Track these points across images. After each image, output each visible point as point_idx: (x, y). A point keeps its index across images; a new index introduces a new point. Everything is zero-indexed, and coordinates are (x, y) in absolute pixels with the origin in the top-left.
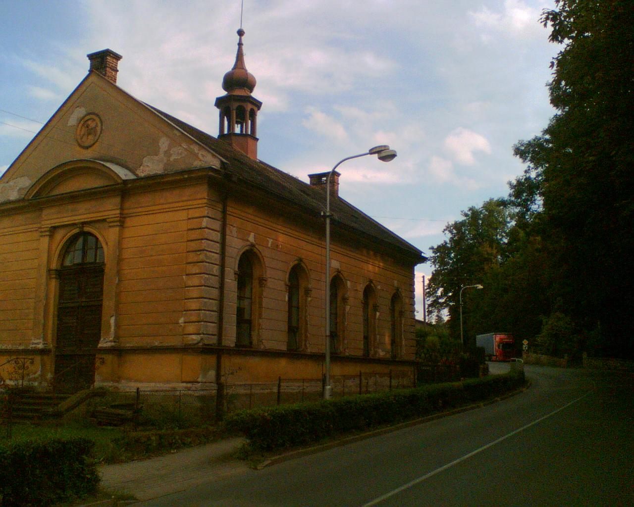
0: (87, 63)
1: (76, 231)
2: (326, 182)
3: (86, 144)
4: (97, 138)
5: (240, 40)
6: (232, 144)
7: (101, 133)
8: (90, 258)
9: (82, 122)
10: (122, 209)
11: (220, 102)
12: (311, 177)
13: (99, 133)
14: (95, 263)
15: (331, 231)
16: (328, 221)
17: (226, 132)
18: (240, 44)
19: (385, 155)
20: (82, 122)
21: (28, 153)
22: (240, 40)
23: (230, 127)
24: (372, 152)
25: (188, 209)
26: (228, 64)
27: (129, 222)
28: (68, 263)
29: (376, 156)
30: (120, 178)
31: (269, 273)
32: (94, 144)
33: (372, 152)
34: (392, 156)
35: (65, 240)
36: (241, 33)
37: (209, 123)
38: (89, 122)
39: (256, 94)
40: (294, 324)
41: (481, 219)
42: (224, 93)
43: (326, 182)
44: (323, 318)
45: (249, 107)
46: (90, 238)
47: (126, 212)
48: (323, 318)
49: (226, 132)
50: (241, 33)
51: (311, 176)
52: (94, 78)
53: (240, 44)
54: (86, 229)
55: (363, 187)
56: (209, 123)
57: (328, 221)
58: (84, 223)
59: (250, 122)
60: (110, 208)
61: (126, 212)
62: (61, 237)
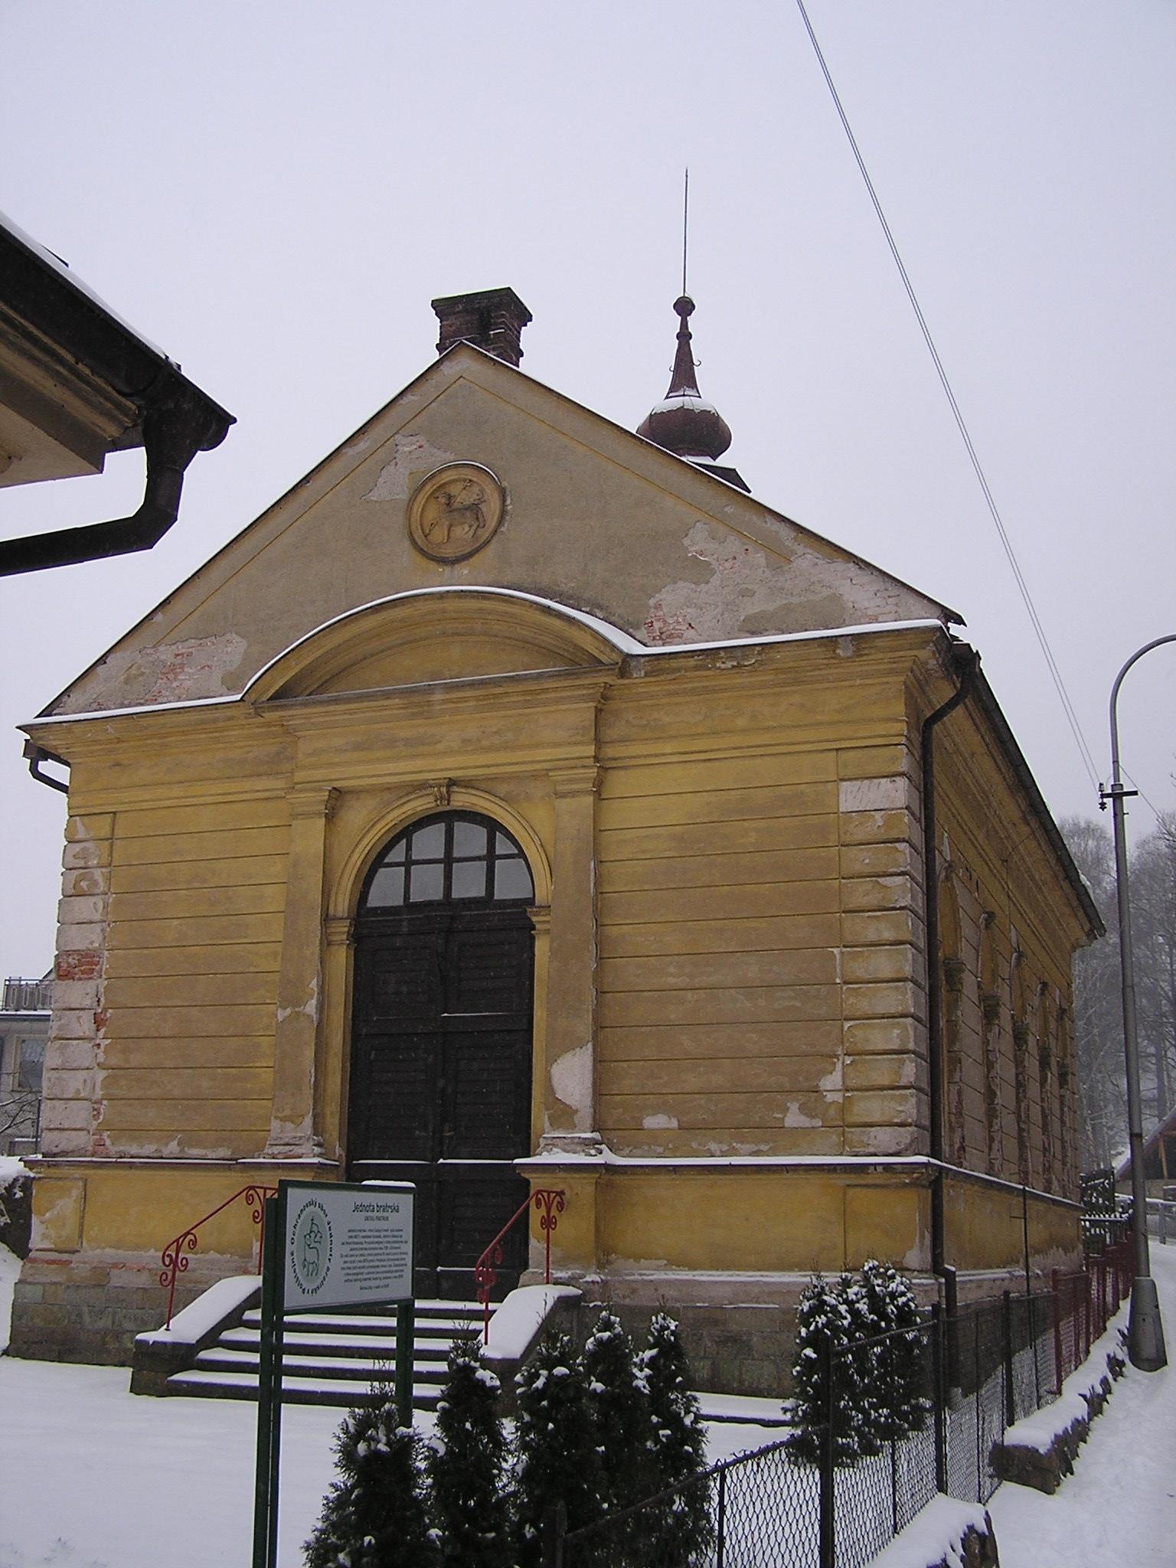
0: (432, 327)
3: (449, 552)
4: (485, 534)
5: (684, 325)
6: (836, 598)
7: (501, 521)
9: (428, 489)
10: (598, 742)
13: (492, 523)
18: (684, 336)
20: (428, 489)
21: (215, 573)
22: (684, 325)
25: (837, 750)
27: (619, 783)
30: (618, 649)
32: (471, 555)
36: (684, 307)
40: (1136, 1131)
44: (406, 1333)
47: (610, 751)
48: (406, 1333)
50: (684, 307)
52: (464, 364)
53: (684, 336)
61: (610, 751)
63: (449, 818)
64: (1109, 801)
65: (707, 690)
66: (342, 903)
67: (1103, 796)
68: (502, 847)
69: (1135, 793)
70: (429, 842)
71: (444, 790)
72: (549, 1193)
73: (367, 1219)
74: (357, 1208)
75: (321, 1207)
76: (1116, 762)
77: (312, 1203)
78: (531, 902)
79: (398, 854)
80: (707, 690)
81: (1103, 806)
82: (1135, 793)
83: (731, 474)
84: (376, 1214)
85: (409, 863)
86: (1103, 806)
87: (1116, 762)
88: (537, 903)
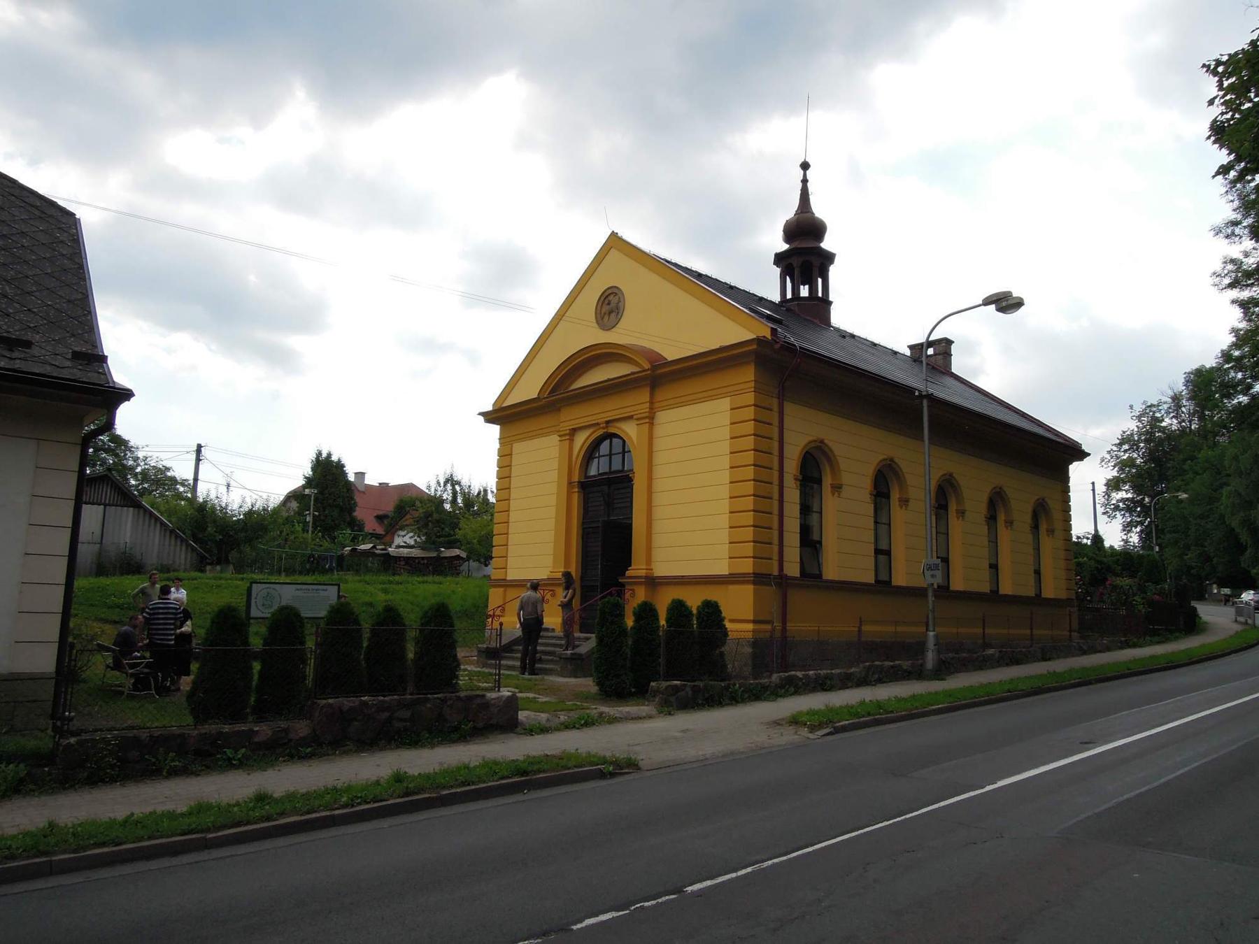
1: (601, 432)
2: (934, 356)
5: (805, 175)
8: (617, 466)
11: (780, 259)
12: (911, 347)
14: (622, 471)
15: (930, 416)
16: (925, 403)
17: (789, 296)
19: (1005, 303)
22: (805, 175)
23: (795, 291)
24: (987, 302)
26: (789, 211)
28: (593, 471)
29: (993, 307)
31: (846, 478)
33: (987, 302)
34: (1019, 304)
35: (589, 442)
36: (805, 166)
37: (768, 285)
38: (611, 298)
39: (826, 245)
41: (255, 656)
42: (786, 247)
43: (934, 356)
45: (816, 262)
46: (615, 440)
49: (789, 296)
50: (805, 166)
51: (911, 347)
54: (612, 430)
55: (995, 367)
56: (768, 285)
57: (925, 403)
58: (607, 422)
59: (820, 280)
60: (638, 401)
62: (581, 439)
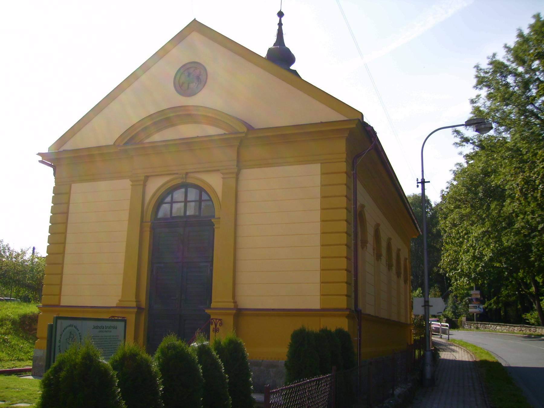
5: (280, 20)
18: (280, 24)
22: (280, 20)
40: (427, 300)
50: (281, 14)
53: (280, 24)
63: (186, 186)
64: (420, 185)
65: (236, 133)
66: (148, 217)
67: (418, 183)
68: (205, 197)
69: (429, 182)
70: (179, 195)
71: (184, 176)
72: (216, 319)
73: (100, 332)
74: (95, 327)
75: (76, 327)
76: (423, 171)
77: (71, 326)
78: (213, 217)
79: (168, 199)
80: (236, 133)
81: (418, 186)
82: (429, 182)
83: (295, 72)
84: (105, 330)
85: (172, 202)
86: (418, 186)
87: (423, 171)
88: (216, 217)
